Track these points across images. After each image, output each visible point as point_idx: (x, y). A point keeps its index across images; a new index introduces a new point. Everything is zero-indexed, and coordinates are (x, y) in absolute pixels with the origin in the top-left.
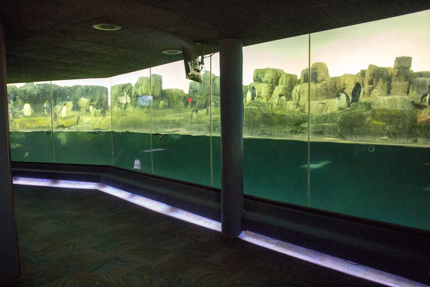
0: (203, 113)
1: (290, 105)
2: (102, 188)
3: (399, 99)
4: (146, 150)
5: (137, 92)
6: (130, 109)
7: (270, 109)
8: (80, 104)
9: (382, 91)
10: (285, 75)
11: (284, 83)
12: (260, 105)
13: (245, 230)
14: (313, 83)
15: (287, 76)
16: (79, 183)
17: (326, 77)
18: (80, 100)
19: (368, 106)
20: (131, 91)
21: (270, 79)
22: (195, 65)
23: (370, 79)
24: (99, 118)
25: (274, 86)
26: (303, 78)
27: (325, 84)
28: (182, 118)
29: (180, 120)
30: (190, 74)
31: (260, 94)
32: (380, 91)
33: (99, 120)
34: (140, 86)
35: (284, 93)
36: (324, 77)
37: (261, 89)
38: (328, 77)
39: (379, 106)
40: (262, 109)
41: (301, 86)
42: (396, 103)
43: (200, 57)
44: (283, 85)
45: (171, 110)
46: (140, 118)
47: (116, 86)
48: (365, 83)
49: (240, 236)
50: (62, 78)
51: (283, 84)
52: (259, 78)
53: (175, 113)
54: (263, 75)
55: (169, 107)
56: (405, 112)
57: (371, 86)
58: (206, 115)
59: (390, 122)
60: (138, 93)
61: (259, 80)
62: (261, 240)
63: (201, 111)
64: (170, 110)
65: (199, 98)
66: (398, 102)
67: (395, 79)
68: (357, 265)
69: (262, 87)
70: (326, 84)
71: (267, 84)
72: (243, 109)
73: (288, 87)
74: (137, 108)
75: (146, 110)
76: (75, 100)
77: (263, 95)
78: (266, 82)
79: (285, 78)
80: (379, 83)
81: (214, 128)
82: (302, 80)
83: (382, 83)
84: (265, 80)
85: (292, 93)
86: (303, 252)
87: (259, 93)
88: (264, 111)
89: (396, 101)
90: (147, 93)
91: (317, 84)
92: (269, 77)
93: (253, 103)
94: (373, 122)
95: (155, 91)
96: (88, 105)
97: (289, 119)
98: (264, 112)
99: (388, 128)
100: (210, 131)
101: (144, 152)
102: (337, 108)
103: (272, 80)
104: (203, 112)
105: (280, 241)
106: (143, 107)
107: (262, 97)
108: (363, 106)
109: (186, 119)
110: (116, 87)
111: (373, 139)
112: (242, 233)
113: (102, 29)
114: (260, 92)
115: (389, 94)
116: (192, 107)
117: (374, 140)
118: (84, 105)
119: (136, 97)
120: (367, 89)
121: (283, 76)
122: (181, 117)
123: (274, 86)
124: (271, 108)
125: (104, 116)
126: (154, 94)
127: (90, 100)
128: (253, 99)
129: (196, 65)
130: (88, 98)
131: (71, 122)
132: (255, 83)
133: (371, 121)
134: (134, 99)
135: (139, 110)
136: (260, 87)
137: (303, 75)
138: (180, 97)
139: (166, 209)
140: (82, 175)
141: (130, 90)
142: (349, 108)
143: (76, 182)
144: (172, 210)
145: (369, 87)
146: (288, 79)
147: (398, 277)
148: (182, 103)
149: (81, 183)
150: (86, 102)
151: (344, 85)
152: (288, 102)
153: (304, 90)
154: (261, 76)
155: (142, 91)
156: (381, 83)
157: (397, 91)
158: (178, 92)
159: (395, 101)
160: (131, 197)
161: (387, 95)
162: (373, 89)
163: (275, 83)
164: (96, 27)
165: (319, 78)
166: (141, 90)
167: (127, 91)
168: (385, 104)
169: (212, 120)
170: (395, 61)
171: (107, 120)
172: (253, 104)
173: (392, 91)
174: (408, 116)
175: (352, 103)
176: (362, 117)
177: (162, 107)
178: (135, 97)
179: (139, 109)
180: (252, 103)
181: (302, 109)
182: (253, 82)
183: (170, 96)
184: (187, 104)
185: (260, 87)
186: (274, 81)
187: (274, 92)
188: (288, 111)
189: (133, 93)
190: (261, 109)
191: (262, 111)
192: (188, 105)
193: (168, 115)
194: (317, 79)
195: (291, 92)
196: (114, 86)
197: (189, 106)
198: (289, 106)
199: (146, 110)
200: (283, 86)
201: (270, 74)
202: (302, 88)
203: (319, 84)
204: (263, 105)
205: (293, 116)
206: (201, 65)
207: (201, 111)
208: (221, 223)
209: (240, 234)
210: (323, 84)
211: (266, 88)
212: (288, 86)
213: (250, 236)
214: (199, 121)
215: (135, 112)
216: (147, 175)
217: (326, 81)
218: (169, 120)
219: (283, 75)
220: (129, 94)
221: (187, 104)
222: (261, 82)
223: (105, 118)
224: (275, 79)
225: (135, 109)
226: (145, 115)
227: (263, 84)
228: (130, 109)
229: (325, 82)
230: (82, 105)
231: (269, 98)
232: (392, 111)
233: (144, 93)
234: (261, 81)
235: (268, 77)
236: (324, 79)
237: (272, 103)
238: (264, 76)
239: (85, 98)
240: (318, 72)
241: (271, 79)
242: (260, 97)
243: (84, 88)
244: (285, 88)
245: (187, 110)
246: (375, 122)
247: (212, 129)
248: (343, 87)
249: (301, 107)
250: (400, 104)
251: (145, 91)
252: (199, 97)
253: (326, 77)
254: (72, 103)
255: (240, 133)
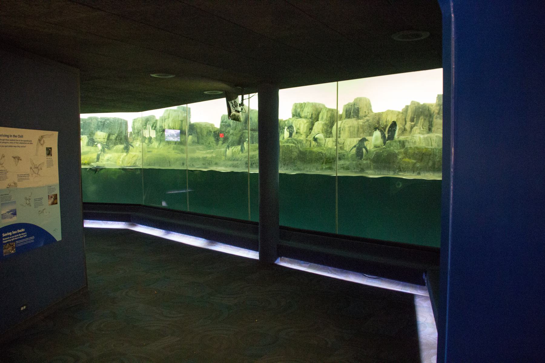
0: (237, 150)
1: (329, 143)
2: (132, 227)
3: (435, 137)
4: (171, 191)
5: (163, 126)
6: (155, 144)
7: (308, 147)
8: (96, 139)
9: (423, 128)
10: (326, 109)
11: (325, 118)
12: (298, 143)
13: (281, 257)
14: (355, 119)
15: (328, 111)
16: (106, 223)
17: (369, 113)
18: (96, 133)
19: (403, 144)
20: (155, 124)
21: (310, 114)
22: (235, 107)
23: (412, 116)
24: (122, 155)
25: (313, 121)
26: (344, 113)
27: (368, 120)
28: (214, 155)
29: (212, 157)
30: (232, 114)
31: (298, 130)
32: (420, 128)
33: (122, 157)
34: (167, 119)
35: (325, 129)
36: (367, 113)
37: (300, 124)
38: (372, 113)
39: (415, 144)
40: (300, 147)
41: (342, 122)
42: (432, 141)
43: (240, 97)
44: (324, 120)
45: (200, 146)
46: (168, 155)
47: (139, 119)
48: (407, 120)
49: (276, 262)
50: (92, 111)
51: (324, 120)
52: (298, 112)
53: (204, 149)
54: (302, 109)
55: (198, 143)
56: (435, 150)
57: (413, 123)
58: (241, 152)
59: (421, 160)
60: (164, 127)
61: (298, 115)
62: (294, 265)
63: (234, 148)
64: (200, 147)
65: (232, 133)
66: (433, 140)
67: (437, 116)
68: (376, 278)
69: (301, 123)
70: (369, 120)
71: (307, 119)
72: (279, 147)
73: (328, 123)
74: (163, 144)
75: (174, 146)
76: (90, 134)
77: (302, 131)
78: (305, 117)
79: (326, 113)
80: (420, 120)
81: (251, 165)
82: (344, 116)
83: (422, 120)
84: (304, 115)
85: (333, 129)
86: (331, 272)
87: (298, 129)
88: (301, 148)
89: (432, 139)
90: (174, 128)
91: (360, 121)
92: (308, 111)
93: (290, 140)
94: (404, 160)
95: (183, 125)
96: (105, 139)
97: (326, 156)
98: (301, 149)
99: (418, 165)
100: (248, 167)
101: (168, 194)
102: (373, 146)
103: (312, 115)
104: (237, 149)
105: (312, 264)
106: (169, 143)
107: (301, 133)
108: (397, 144)
109: (218, 156)
110: (139, 120)
111: (388, 172)
112: (277, 260)
113: (158, 77)
114: (299, 128)
115: (430, 132)
116: (224, 143)
117: (389, 174)
118: (100, 139)
119: (162, 131)
120: (409, 126)
121: (324, 111)
122: (212, 155)
123: (314, 122)
124: (310, 146)
125: (127, 152)
126: (182, 128)
127: (107, 135)
128: (291, 135)
129: (237, 106)
130: (105, 132)
131: (88, 159)
132: (294, 118)
133: (403, 158)
134: (159, 134)
135: (165, 146)
136: (299, 122)
137: (345, 110)
138: (210, 132)
139: (204, 243)
140: (112, 214)
141: (155, 123)
142: (384, 146)
143: (103, 221)
144: (210, 244)
145: (411, 124)
146: (329, 115)
147: (405, 283)
148: (212, 139)
149: (108, 223)
150: (103, 136)
151: (386, 122)
152: (327, 139)
153: (344, 126)
154: (300, 110)
155: (168, 125)
156: (421, 120)
157: (438, 128)
158: (208, 126)
159: (431, 139)
160: (166, 235)
161: (428, 133)
162: (414, 125)
163: (315, 118)
164: (154, 75)
165: (361, 114)
166: (167, 124)
167: (152, 125)
168: (421, 142)
169: (249, 157)
170: (437, 97)
171: (131, 157)
172: (290, 141)
173: (433, 129)
174: (437, 154)
175: (387, 140)
176: (395, 155)
177: (191, 143)
178: (160, 131)
179: (165, 144)
180: (289, 140)
181: (341, 147)
182: (291, 117)
183: (198, 130)
184: (217, 140)
185: (299, 122)
186: (314, 116)
187: (314, 128)
188: (325, 148)
189: (158, 127)
190: (299, 146)
191: (299, 148)
192: (219, 141)
193: (197, 151)
194: (359, 115)
195: (332, 128)
196: (137, 118)
197: (220, 142)
198: (328, 143)
199: (173, 145)
200: (324, 121)
201: (309, 109)
202: (342, 124)
203: (361, 120)
204: (300, 142)
205: (330, 153)
206: (241, 106)
207: (234, 148)
208: (258, 252)
209: (276, 260)
210: (366, 121)
211: (305, 124)
212: (329, 122)
213: (285, 262)
214: (234, 159)
215: (160, 148)
216: (184, 212)
217: (369, 116)
218: (200, 157)
219: (324, 110)
220: (153, 128)
221: (217, 140)
222: (301, 117)
223: (129, 154)
224: (315, 114)
225: (161, 144)
226: (174, 151)
227: (302, 120)
228: (154, 145)
229: (367, 118)
230: (98, 139)
231: (308, 134)
232: (423, 149)
233: (171, 127)
234: (299, 116)
235: (307, 112)
236: (366, 115)
237: (311, 141)
238: (303, 111)
239: (102, 131)
240: (360, 107)
241: (311, 114)
242: (298, 134)
243: (100, 120)
244: (326, 124)
245: (218, 146)
246: (407, 160)
247: (250, 165)
248: (385, 124)
249: (341, 144)
250: (435, 142)
251: (173, 125)
252: (232, 132)
253: (369, 113)
254: (88, 137)
255: (276, 169)
